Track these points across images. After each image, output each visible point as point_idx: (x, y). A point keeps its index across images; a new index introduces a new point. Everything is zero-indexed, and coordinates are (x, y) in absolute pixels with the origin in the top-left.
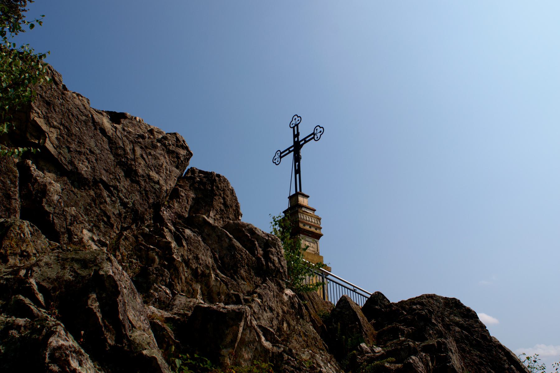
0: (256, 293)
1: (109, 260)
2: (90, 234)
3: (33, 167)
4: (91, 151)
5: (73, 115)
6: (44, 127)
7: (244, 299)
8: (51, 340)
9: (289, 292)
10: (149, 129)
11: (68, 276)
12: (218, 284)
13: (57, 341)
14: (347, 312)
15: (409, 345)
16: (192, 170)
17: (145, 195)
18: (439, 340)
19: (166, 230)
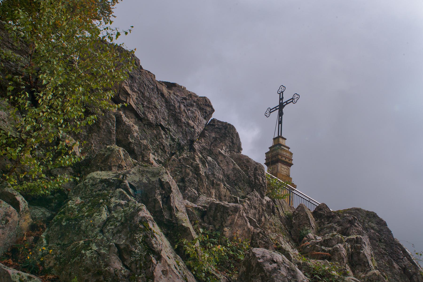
0: (247, 197)
1: (166, 173)
2: (153, 156)
3: (123, 116)
4: (155, 107)
5: (146, 85)
6: (129, 92)
7: (240, 200)
8: (140, 213)
9: (267, 198)
10: (189, 94)
11: (145, 181)
12: (225, 190)
13: (143, 214)
14: (302, 214)
15: (338, 237)
16: (213, 120)
17: (185, 134)
18: (358, 236)
19: (196, 156)
